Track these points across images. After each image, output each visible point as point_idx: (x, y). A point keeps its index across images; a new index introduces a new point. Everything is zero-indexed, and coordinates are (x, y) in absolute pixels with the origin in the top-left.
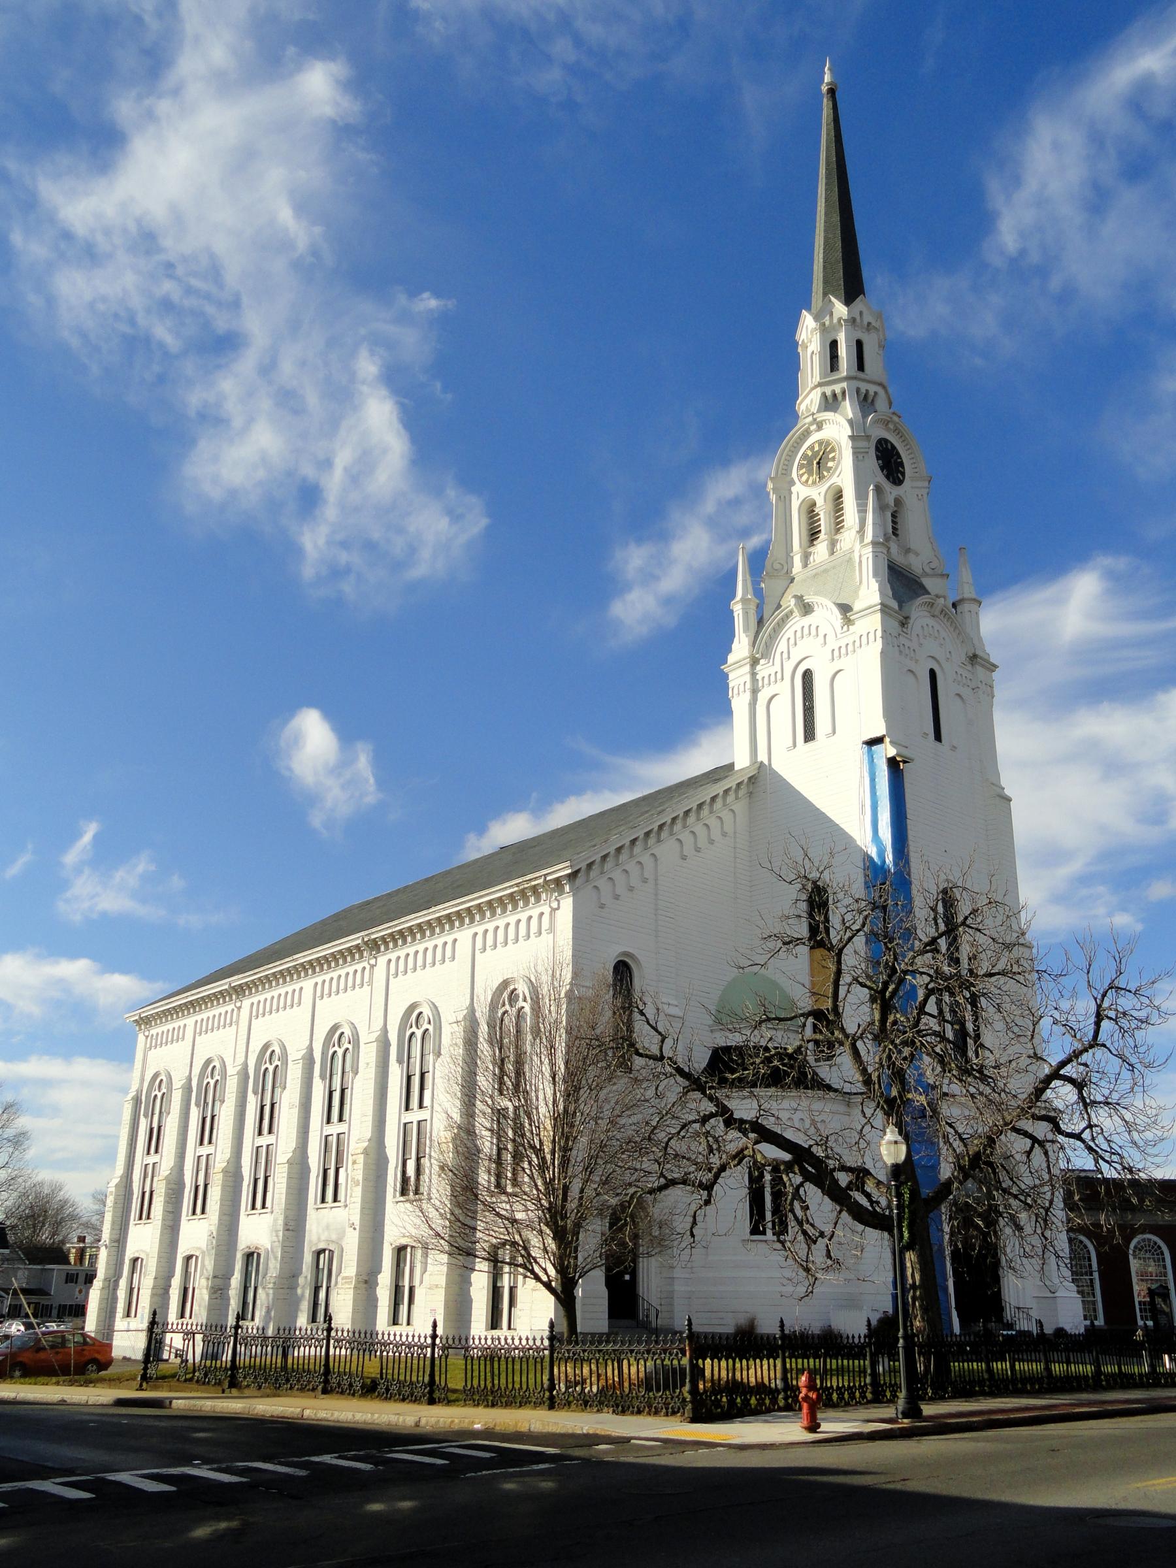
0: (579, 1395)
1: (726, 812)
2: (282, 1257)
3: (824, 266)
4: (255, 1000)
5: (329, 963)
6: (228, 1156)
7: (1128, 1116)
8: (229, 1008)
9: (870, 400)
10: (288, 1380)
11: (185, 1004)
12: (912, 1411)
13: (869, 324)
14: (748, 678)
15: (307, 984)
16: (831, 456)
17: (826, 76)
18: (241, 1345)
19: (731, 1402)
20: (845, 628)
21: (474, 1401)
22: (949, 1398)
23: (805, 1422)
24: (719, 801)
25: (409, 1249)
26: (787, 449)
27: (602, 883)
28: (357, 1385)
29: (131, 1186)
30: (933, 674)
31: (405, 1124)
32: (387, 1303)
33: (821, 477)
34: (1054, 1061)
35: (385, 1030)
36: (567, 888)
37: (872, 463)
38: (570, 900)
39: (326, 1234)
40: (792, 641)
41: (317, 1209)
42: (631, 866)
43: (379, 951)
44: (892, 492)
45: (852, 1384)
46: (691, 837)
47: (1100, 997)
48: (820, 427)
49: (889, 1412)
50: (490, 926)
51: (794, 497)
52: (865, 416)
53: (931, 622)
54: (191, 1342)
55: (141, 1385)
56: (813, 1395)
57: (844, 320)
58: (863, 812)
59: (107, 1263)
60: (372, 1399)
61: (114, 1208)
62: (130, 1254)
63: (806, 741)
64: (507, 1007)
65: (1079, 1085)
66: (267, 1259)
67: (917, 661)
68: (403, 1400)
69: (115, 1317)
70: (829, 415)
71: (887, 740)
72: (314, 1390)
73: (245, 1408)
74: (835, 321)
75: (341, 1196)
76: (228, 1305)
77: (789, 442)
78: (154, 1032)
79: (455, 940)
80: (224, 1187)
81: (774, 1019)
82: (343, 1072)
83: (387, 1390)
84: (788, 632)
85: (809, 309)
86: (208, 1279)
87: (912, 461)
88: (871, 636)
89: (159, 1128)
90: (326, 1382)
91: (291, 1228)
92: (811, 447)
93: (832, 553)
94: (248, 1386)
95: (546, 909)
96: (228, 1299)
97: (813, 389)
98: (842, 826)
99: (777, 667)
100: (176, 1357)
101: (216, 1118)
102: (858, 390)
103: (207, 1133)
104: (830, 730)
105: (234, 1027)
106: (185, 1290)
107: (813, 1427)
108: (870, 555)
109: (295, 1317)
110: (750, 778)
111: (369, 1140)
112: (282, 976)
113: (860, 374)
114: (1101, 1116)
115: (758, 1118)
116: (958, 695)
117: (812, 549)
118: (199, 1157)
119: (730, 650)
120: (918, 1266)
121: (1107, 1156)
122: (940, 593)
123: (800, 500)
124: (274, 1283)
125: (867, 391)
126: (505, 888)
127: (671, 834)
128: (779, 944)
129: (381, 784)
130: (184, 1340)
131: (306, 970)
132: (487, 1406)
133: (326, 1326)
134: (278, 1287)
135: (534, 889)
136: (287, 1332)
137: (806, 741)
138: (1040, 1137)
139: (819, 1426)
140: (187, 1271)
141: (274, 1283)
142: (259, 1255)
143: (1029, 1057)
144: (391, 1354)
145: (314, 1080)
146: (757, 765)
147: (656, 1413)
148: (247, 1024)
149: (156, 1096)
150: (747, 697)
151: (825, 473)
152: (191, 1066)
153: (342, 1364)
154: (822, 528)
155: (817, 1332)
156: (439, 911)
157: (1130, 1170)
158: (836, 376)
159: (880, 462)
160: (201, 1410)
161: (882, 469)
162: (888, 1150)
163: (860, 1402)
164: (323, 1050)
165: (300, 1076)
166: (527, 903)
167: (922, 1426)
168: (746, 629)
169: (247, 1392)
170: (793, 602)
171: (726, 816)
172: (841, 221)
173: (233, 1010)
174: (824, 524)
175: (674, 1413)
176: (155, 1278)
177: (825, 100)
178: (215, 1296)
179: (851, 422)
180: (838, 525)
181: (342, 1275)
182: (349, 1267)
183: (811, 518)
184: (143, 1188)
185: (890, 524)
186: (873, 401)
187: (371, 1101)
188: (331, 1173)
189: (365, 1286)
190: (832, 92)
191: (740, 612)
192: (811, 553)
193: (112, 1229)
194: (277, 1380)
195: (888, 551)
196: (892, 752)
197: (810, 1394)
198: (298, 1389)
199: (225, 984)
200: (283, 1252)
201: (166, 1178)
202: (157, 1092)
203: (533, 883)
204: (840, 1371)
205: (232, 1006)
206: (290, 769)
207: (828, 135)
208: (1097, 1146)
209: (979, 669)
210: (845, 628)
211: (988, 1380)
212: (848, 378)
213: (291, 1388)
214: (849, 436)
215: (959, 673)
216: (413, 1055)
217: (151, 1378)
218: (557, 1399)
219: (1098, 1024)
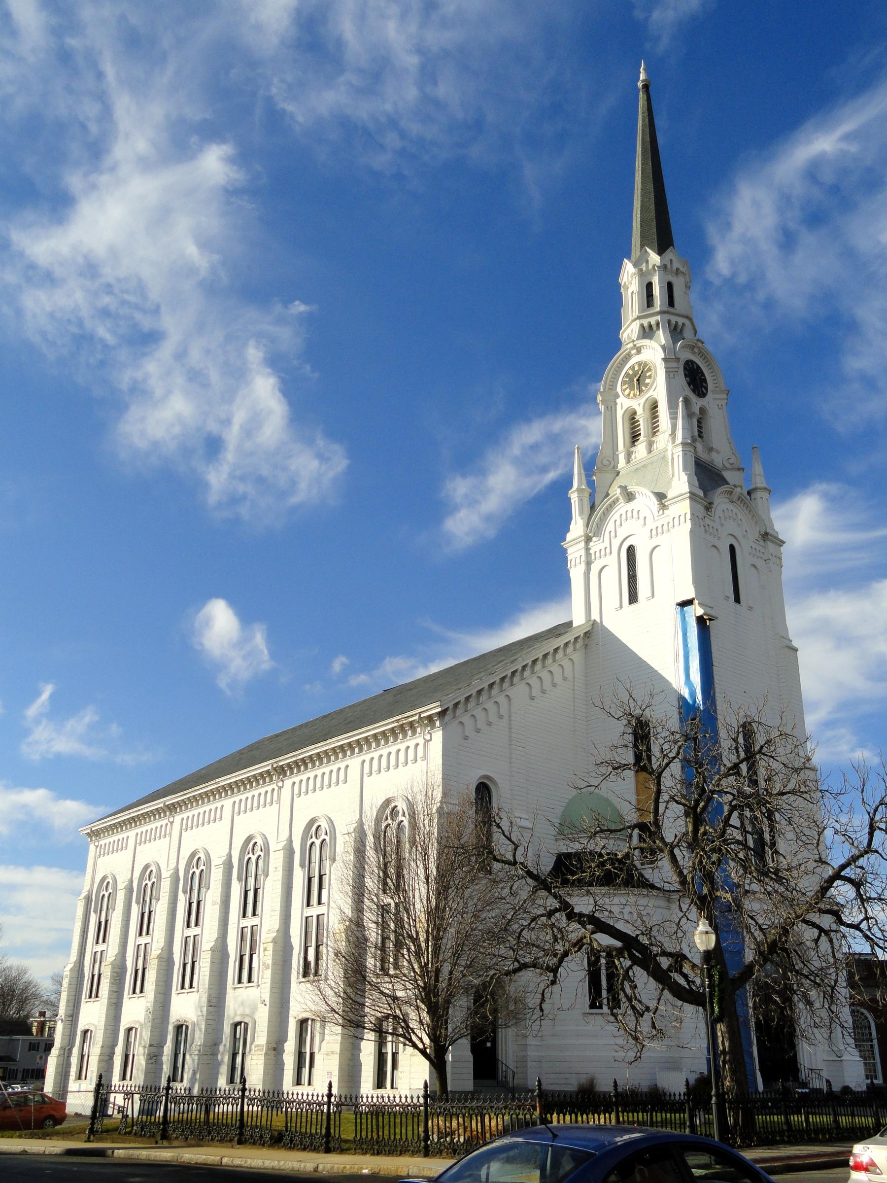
2: (206, 1029)
6: (162, 944)
9: (679, 330)
10: (209, 1133)
13: (678, 269)
14: (583, 552)
15: (227, 803)
18: (171, 1103)
20: (661, 511)
21: (363, 1149)
22: (756, 1146)
24: (561, 652)
25: (310, 1022)
27: (466, 719)
28: (267, 1137)
29: (83, 970)
30: (732, 548)
35: (290, 841)
36: (438, 723)
37: (681, 379)
40: (618, 523)
41: (235, 988)
42: (490, 705)
43: (285, 775)
44: (697, 403)
47: (872, 811)
48: (639, 351)
51: (619, 407)
53: (731, 507)
54: (130, 1101)
55: (89, 1138)
58: (677, 660)
59: (63, 1034)
60: (279, 1148)
61: (69, 988)
62: (81, 1027)
63: (630, 603)
65: (857, 884)
66: (194, 1030)
68: (304, 1149)
69: (68, 1079)
70: (646, 342)
71: (696, 602)
72: (231, 1141)
74: (650, 267)
75: (255, 977)
76: (162, 1069)
78: (102, 842)
79: (347, 766)
82: (256, 875)
83: (291, 1141)
84: (615, 516)
85: (629, 258)
88: (682, 518)
89: (106, 921)
91: (213, 1005)
92: (632, 368)
93: (650, 452)
95: (421, 741)
98: (660, 672)
99: (607, 544)
100: (118, 1113)
102: (669, 322)
103: (145, 926)
104: (650, 595)
105: (275, 806)
108: (681, 454)
110: (586, 633)
111: (278, 931)
113: (671, 310)
115: (594, 912)
117: (633, 449)
119: (568, 530)
120: (727, 1035)
123: (624, 408)
125: (676, 322)
126: (388, 724)
127: (522, 679)
128: (610, 769)
130: (125, 1099)
132: (373, 1154)
133: (241, 1086)
135: (411, 724)
136: (209, 1092)
137: (630, 603)
138: (826, 927)
140: (128, 1041)
141: (199, 1051)
142: (187, 1027)
143: (816, 861)
145: (233, 881)
146: (591, 623)
149: (104, 895)
150: (582, 567)
151: (644, 388)
154: (642, 432)
156: (333, 743)
158: (651, 311)
159: (688, 379)
160: (138, 1159)
161: (689, 384)
162: (701, 939)
164: (240, 857)
165: (221, 878)
166: (405, 736)
170: (618, 491)
171: (566, 663)
173: (167, 824)
174: (643, 428)
176: (102, 1047)
177: (641, 93)
178: (150, 1061)
179: (664, 348)
180: (654, 429)
181: (255, 1043)
182: (261, 1037)
185: (696, 429)
186: (682, 330)
188: (246, 959)
189: (274, 1052)
190: (646, 87)
191: (576, 499)
193: (67, 1006)
194: (200, 1132)
196: (700, 612)
198: (218, 1141)
199: (161, 803)
200: (207, 1025)
201: (112, 964)
202: (104, 892)
203: (410, 720)
205: (166, 821)
207: (643, 121)
208: (872, 934)
210: (661, 511)
212: (661, 313)
213: (212, 1140)
214: (663, 359)
215: (758, 549)
216: (313, 861)
217: (97, 1131)
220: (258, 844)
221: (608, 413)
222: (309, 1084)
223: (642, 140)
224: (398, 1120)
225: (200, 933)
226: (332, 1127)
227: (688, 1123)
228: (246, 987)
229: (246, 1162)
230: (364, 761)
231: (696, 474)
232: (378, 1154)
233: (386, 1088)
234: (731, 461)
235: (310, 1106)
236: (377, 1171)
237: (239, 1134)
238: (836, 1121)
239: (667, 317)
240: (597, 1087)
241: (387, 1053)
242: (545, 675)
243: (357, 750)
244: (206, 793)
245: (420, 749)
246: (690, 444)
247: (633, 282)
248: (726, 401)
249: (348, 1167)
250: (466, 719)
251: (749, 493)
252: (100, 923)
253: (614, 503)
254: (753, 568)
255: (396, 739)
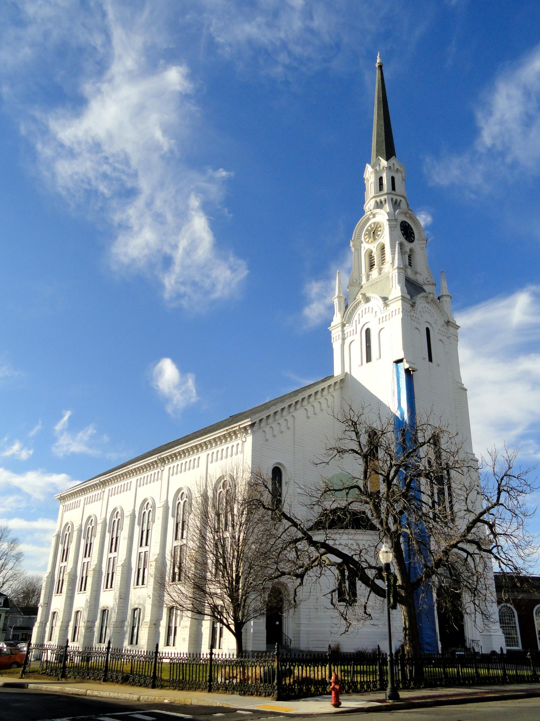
0: (223, 684)
1: (329, 396)
2: (118, 612)
3: (377, 144)
4: (110, 488)
5: (143, 469)
7: (516, 541)
8: (99, 491)
10: (88, 674)
11: (80, 490)
12: (394, 696)
13: (397, 169)
15: (134, 480)
16: (379, 229)
17: (378, 60)
19: (301, 690)
20: (385, 308)
21: (174, 687)
22: (423, 688)
23: (333, 702)
24: (326, 390)
26: (359, 227)
27: (267, 429)
28: (120, 678)
29: (54, 577)
30: (428, 330)
31: (175, 547)
32: (164, 635)
33: (375, 239)
34: (478, 512)
36: (249, 431)
37: (398, 232)
38: (251, 437)
39: (138, 600)
40: (361, 315)
41: (135, 588)
42: (282, 421)
43: (165, 464)
44: (408, 246)
45: (375, 680)
46: (312, 408)
47: (500, 480)
48: (374, 216)
49: (382, 696)
50: (215, 450)
51: (362, 249)
52: (395, 211)
53: (427, 305)
54: (46, 654)
55: (22, 676)
56: (337, 687)
57: (386, 168)
58: (393, 395)
60: (126, 685)
62: (52, 610)
63: (367, 362)
64: (222, 490)
65: (491, 527)
66: (111, 613)
67: (420, 324)
68: (141, 686)
70: (378, 210)
71: (405, 360)
73: (60, 689)
74: (381, 168)
75: (145, 582)
76: (94, 635)
77: (358, 226)
78: (67, 503)
79: (199, 458)
80: (93, 577)
81: (332, 490)
82: (148, 522)
83: (134, 680)
84: (359, 311)
85: (370, 163)
86: (85, 622)
87: (417, 230)
88: (397, 311)
89: (68, 549)
90: (106, 675)
91: (122, 598)
92: (370, 226)
93: (380, 274)
94: (70, 677)
95: (240, 442)
96: (94, 633)
97: (371, 199)
99: (354, 328)
101: (92, 544)
102: (392, 199)
103: (88, 552)
104: (378, 357)
105: (159, 481)
106: (76, 628)
107: (337, 704)
108: (397, 274)
109: (123, 642)
110: (341, 380)
112: (123, 476)
113: (393, 192)
114: (501, 540)
115: (325, 541)
116: (441, 340)
118: (84, 563)
120: (407, 618)
121: (505, 561)
122: (431, 292)
123: (366, 250)
124: (114, 625)
125: (396, 199)
126: (221, 432)
127: (302, 406)
128: (336, 452)
129: (198, 393)
131: (133, 473)
132: (179, 690)
134: (115, 627)
135: (235, 432)
136: (89, 649)
137: (367, 362)
138: (471, 551)
139: (340, 704)
140: (76, 618)
141: (114, 625)
142: (108, 611)
143: (465, 510)
144: (125, 660)
146: (344, 374)
147: (260, 695)
148: (107, 499)
149: (89, 528)
150: (340, 342)
151: (377, 237)
152: (82, 519)
153: (114, 666)
154: (376, 263)
155: (370, 651)
157: (516, 569)
158: (382, 193)
159: (402, 232)
160: (41, 690)
161: (403, 235)
162: (383, 556)
163: (373, 690)
165: (129, 523)
166: (231, 439)
167: (399, 704)
168: (340, 310)
169: (69, 680)
170: (361, 296)
171: (329, 398)
172: (384, 123)
173: (101, 493)
174: (376, 261)
175: (269, 695)
176: (62, 622)
177: (377, 70)
178: (87, 631)
179: (388, 214)
180: (383, 260)
181: (144, 621)
182: (147, 617)
183: (371, 258)
184: (59, 578)
185: (407, 261)
186: (399, 204)
187: (160, 536)
190: (380, 67)
191: (337, 302)
192: (370, 275)
193: (45, 598)
194: (83, 674)
195: (405, 272)
196: (407, 366)
197: (336, 687)
198: (93, 679)
199: (98, 480)
200: (118, 609)
201: (69, 573)
202: (67, 532)
203: (234, 429)
204: (362, 673)
205: (101, 491)
206: (157, 386)
207: (378, 86)
208: (501, 556)
209: (451, 328)
210: (385, 308)
211: (444, 678)
212: (387, 194)
213: (90, 679)
214: (387, 220)
215: (443, 331)
217: (27, 672)
218: (213, 686)
219: (499, 494)
220: (150, 504)
221: (356, 252)
222: (174, 645)
223: (378, 96)
224: (201, 668)
225: (117, 556)
226: (157, 672)
227: (378, 673)
228: (141, 588)
229: (100, 694)
230: (208, 454)
231: (406, 286)
232: (182, 690)
233: (216, 648)
234: (428, 280)
235: (139, 658)
236: (173, 701)
237: (104, 675)
238: (477, 672)
239: (391, 196)
240: (342, 649)
241: (217, 627)
242: (316, 404)
243: (204, 448)
244: (122, 474)
245: (240, 446)
246: (402, 268)
247: (372, 177)
248: (425, 245)
249: (157, 698)
250: (267, 429)
251: (439, 298)
252: (64, 550)
253: (358, 303)
254: (440, 342)
255: (226, 441)
